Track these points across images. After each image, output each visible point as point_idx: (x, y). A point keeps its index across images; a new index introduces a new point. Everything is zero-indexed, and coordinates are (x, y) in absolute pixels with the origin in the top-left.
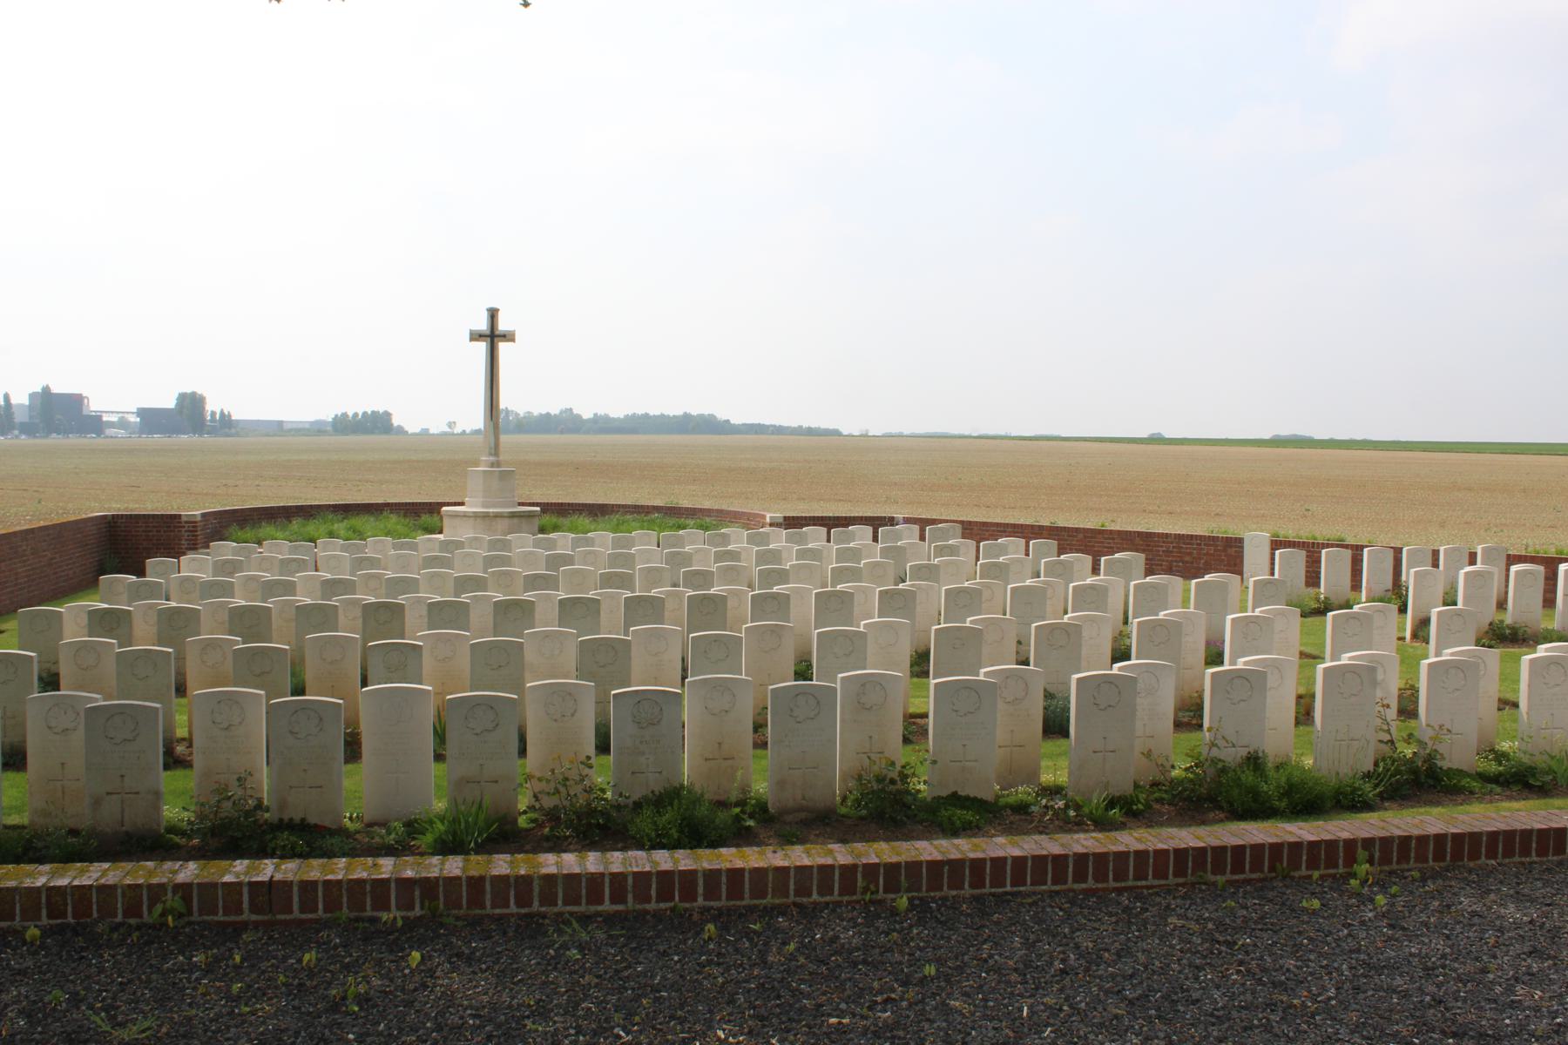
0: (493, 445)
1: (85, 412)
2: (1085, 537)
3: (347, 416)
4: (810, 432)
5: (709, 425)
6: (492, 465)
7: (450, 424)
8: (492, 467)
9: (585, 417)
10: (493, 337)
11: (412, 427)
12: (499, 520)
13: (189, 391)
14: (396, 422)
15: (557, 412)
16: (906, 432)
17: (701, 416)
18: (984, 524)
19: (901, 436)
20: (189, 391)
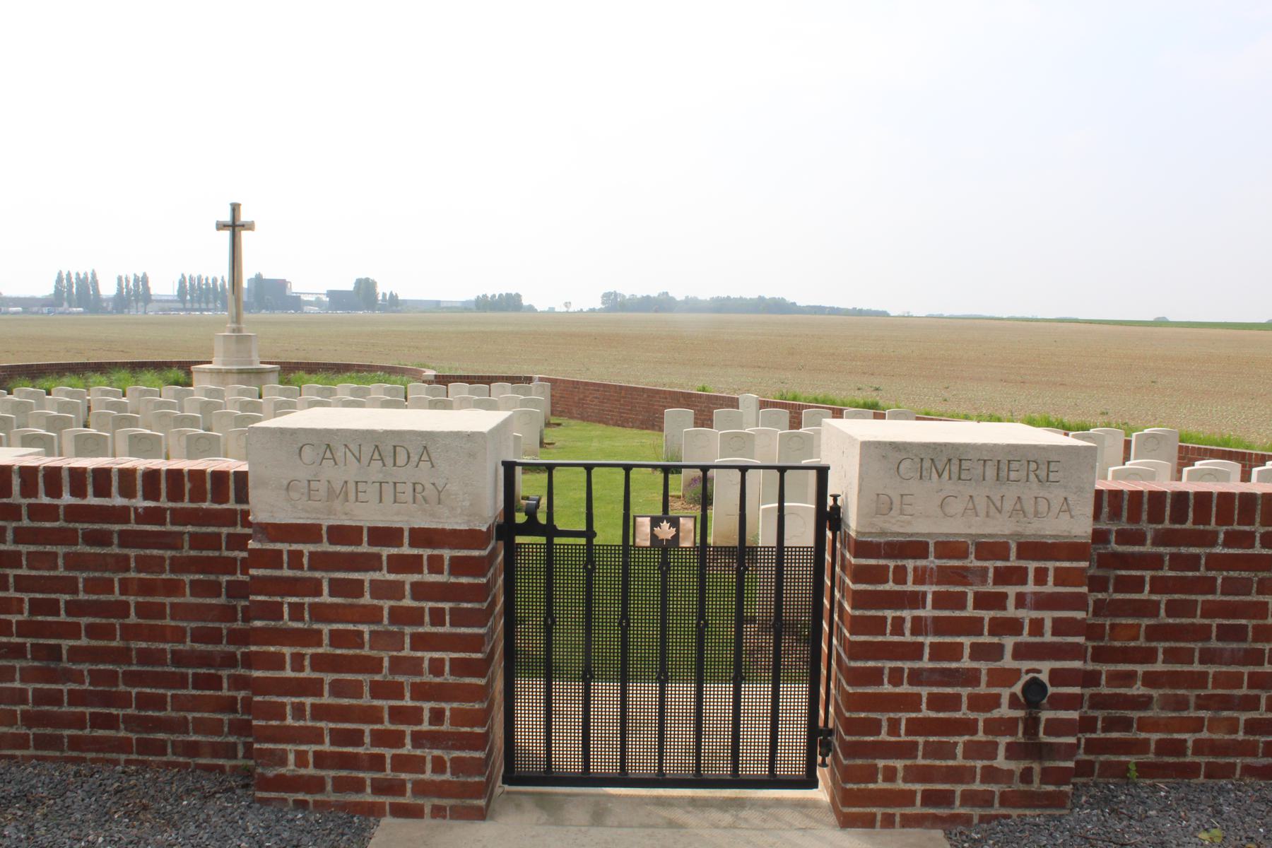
0: (234, 314)
1: (288, 293)
2: (649, 396)
3: (487, 297)
4: (860, 313)
5: (779, 306)
6: (234, 331)
7: (567, 304)
8: (233, 332)
9: (678, 299)
10: (235, 226)
11: (541, 306)
12: (230, 375)
13: (364, 277)
14: (525, 302)
15: (656, 295)
16: (946, 314)
17: (750, 299)
18: (586, 384)
19: (941, 317)
20: (364, 277)
